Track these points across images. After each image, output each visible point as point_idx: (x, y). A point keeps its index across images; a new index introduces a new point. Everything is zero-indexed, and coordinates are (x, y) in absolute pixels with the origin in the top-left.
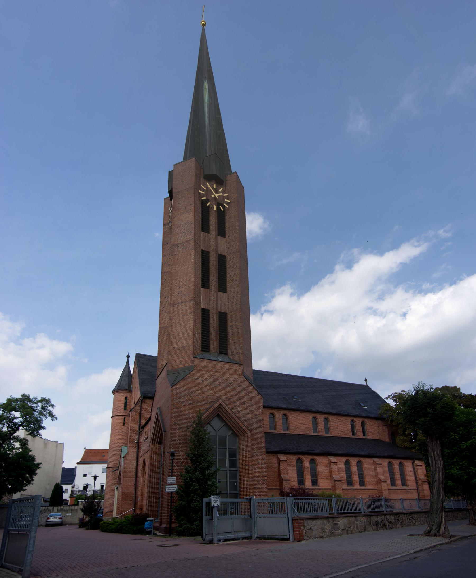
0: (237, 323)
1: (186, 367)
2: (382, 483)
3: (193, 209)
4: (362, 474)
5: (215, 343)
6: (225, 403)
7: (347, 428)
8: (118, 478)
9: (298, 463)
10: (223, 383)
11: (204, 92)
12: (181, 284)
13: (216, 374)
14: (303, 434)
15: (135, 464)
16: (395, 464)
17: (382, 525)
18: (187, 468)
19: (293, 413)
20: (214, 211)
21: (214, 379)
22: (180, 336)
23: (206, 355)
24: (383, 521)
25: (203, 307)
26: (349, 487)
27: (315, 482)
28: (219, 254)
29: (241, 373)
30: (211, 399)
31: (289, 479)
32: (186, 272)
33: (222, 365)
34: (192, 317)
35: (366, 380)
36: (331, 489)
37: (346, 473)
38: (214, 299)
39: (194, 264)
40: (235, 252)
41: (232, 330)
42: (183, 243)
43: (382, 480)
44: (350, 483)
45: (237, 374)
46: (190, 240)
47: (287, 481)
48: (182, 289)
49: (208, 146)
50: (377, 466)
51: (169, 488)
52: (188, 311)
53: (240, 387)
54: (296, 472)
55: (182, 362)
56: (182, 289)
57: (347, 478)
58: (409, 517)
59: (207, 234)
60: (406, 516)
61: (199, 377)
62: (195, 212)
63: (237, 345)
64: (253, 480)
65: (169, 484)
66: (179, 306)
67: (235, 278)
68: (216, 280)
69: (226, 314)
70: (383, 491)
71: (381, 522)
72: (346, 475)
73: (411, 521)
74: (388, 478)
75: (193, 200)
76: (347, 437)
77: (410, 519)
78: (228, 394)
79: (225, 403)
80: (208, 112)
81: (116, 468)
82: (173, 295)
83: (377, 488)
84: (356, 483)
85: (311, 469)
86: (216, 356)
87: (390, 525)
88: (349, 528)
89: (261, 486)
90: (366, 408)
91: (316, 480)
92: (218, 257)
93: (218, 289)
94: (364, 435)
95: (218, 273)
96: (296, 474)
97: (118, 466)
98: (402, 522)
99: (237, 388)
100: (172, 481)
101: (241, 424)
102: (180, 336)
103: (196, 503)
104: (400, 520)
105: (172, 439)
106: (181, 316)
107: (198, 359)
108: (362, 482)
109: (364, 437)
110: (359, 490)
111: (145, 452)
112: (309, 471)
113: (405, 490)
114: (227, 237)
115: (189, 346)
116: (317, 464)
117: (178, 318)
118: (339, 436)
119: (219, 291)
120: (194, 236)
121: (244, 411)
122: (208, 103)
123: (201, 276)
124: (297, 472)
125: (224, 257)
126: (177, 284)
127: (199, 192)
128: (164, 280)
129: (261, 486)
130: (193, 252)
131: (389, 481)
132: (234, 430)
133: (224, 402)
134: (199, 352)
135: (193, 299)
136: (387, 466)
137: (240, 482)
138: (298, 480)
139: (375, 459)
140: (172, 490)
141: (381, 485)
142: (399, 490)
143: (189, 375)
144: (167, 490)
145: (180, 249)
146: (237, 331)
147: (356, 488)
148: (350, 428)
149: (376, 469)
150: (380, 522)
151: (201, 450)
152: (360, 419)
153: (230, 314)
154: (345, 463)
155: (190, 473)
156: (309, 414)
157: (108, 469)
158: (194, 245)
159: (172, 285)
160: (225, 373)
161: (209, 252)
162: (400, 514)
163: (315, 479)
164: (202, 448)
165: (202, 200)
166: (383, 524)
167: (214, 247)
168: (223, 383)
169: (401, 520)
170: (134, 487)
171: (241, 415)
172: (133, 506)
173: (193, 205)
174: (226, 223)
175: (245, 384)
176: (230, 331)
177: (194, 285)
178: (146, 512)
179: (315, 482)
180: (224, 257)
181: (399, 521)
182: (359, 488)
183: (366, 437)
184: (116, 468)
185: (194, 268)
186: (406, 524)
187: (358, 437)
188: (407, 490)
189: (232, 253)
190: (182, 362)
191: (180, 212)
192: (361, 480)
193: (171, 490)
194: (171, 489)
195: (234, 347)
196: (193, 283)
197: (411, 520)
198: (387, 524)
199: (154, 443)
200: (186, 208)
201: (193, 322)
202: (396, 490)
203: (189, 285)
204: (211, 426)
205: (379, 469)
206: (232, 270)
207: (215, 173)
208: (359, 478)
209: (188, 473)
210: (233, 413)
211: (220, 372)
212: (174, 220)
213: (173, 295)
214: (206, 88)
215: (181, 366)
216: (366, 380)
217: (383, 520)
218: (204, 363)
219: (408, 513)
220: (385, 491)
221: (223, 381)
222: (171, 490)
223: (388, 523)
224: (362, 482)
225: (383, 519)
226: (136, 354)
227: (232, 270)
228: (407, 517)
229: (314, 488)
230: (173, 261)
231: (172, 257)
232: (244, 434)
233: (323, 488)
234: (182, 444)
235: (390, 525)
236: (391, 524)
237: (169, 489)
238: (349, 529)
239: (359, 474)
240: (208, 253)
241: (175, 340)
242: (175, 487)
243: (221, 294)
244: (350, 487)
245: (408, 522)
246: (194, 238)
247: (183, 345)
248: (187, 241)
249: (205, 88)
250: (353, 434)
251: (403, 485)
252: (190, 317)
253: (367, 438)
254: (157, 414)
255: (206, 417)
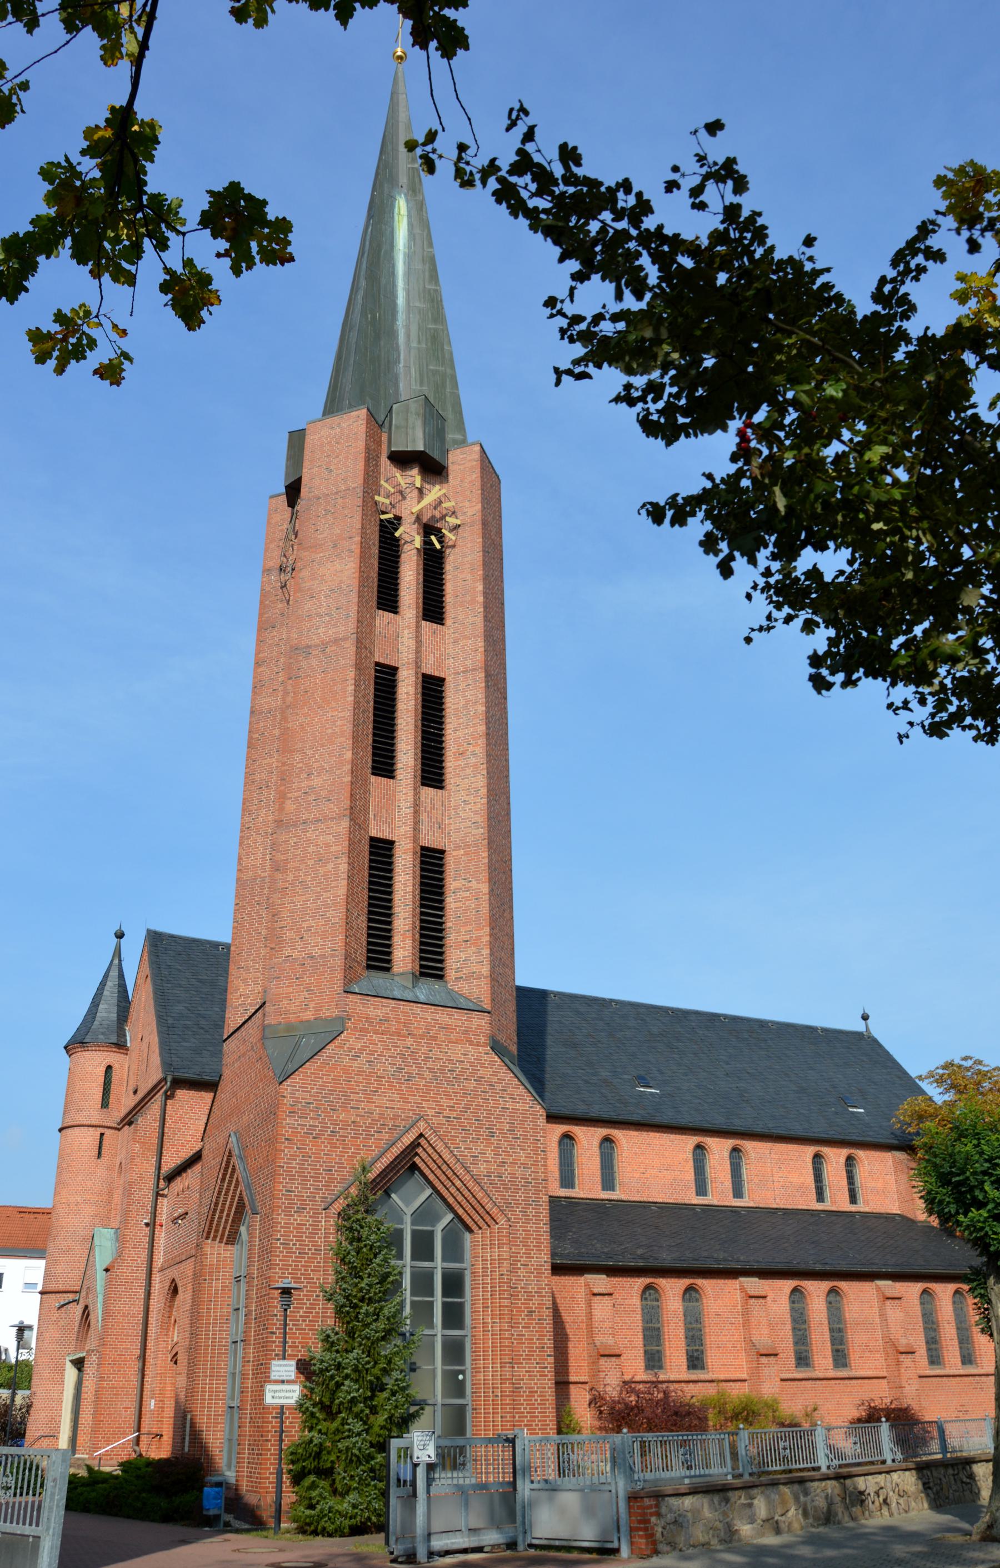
0: (474, 884)
1: (320, 1018)
2: (902, 1358)
3: (358, 551)
4: (840, 1330)
5: (409, 942)
6: (435, 1132)
7: (802, 1180)
8: (76, 1329)
9: (646, 1299)
10: (431, 1070)
11: (396, 223)
12: (314, 765)
13: (410, 1041)
14: (666, 1201)
15: (141, 1293)
16: (941, 1295)
17: (877, 1504)
18: (328, 1336)
19: (636, 1133)
20: (415, 551)
21: (402, 1055)
22: (305, 925)
23: (378, 979)
24: (881, 1491)
25: (374, 833)
26: (801, 1372)
27: (695, 1361)
28: (424, 676)
29: (483, 1040)
30: (395, 1118)
31: (617, 1352)
32: (330, 731)
33: (429, 1014)
34: (344, 867)
35: (865, 1018)
36: (745, 1380)
37: (794, 1329)
38: (408, 811)
39: (355, 709)
40: (472, 670)
41: (460, 904)
42: (325, 645)
43: (902, 1349)
44: (803, 1360)
45: (471, 1043)
46: (345, 639)
47: (614, 1359)
48: (317, 782)
49: (401, 365)
50: (888, 1302)
51: (275, 1391)
52: (333, 849)
53: (479, 1080)
54: (640, 1329)
55: (312, 1005)
56: (317, 782)
57: (796, 1343)
58: (961, 1475)
59: (391, 615)
60: (950, 1471)
61: (361, 1051)
62: (363, 557)
63: (473, 949)
64: (513, 1367)
65: (276, 1382)
66: (304, 831)
67: (471, 748)
68: (416, 754)
69: (443, 852)
70: (904, 1384)
71: (877, 1493)
72: (794, 1335)
73: (966, 1488)
74: (918, 1341)
75: (359, 526)
76: (800, 1207)
77: (962, 1482)
78: (444, 1102)
79: (435, 1132)
80: (404, 274)
81: (71, 1297)
82: (289, 795)
83: (885, 1374)
84: (823, 1361)
85: (685, 1319)
86: (410, 986)
87: (901, 1501)
88: (782, 1515)
89: (536, 1384)
90: (862, 1111)
91: (702, 1352)
92: (423, 681)
93: (419, 778)
94: (853, 1199)
95: (420, 732)
96: (640, 1336)
97: (77, 1288)
98: (938, 1492)
99: (472, 1085)
100: (284, 1374)
101: (480, 1195)
102: (305, 925)
103: (354, 1440)
104: (931, 1484)
105: (279, 1239)
106: (311, 863)
107: (359, 996)
108: (840, 1357)
109: (853, 1208)
110: (833, 1382)
111: (178, 1260)
112: (681, 1324)
113: (971, 1378)
114: (449, 621)
115: (332, 956)
116: (705, 1301)
117: (303, 867)
118: (775, 1206)
119: (423, 784)
120: (358, 627)
121: (490, 1154)
122: (405, 253)
123: (371, 741)
124: (645, 1330)
125: (441, 681)
126: (301, 765)
127: (373, 498)
128: (257, 736)
129: (536, 1384)
130: (351, 674)
131: (922, 1352)
132: (460, 1211)
133: (432, 1128)
134: (360, 969)
135: (347, 812)
136: (917, 1302)
137: (476, 1370)
138: (645, 1352)
139: (881, 1283)
140: (284, 1398)
141: (898, 1363)
142: (951, 1379)
143: (331, 1047)
144: (269, 1400)
145: (314, 663)
146: (473, 906)
147: (820, 1375)
148: (810, 1180)
149: (883, 1315)
150: (872, 1494)
151: (366, 1281)
152: (841, 1150)
153: (454, 853)
154: (790, 1297)
155: (337, 1351)
156: (684, 1137)
157: (45, 1296)
158: (357, 654)
159: (287, 768)
160: (434, 1038)
161: (396, 669)
162: (933, 1469)
163: (697, 1350)
164: (369, 1275)
165: (381, 520)
166: (881, 1499)
167: (410, 656)
168: (431, 1070)
169: (935, 1485)
170: (137, 1365)
171: (481, 1169)
172: (134, 1425)
173: (358, 539)
174: (448, 584)
175: (495, 1074)
176: (453, 905)
177: (352, 772)
178: (183, 1449)
179: (695, 1361)
180: (441, 681)
181: (930, 1488)
182: (831, 1374)
183: (861, 1207)
184: (71, 1297)
185: (354, 720)
186: (951, 1496)
187: (834, 1208)
188: (977, 1378)
189: (463, 672)
190: (312, 1005)
191: (318, 556)
192: (837, 1351)
193: (280, 1398)
194: (281, 1394)
195: (463, 956)
196: (349, 767)
197: (967, 1484)
198: (893, 1498)
199: (214, 1239)
200: (335, 547)
201: (345, 882)
202: (945, 1379)
203: (338, 772)
204: (53, 12)
205: (894, 1312)
206: (462, 721)
207: (422, 449)
208: (833, 1345)
209: (329, 1350)
210: (458, 1160)
211: (422, 1037)
212: (301, 575)
213: (289, 795)
214: (402, 212)
215: (309, 1015)
216: (865, 1018)
217: (882, 1488)
218: (378, 1009)
219: (956, 1464)
220: (911, 1382)
221: (430, 1064)
222: (280, 1398)
223: (897, 1497)
224: (840, 1357)
225: (883, 1485)
226: (149, 931)
227: (462, 721)
228: (954, 1475)
229: (693, 1377)
230: (292, 694)
231: (290, 681)
232: (489, 1226)
233: (722, 1377)
234: (307, 1254)
235: (901, 1501)
236: (905, 1498)
237: (277, 1394)
238: (783, 1518)
239: (831, 1330)
240: (393, 670)
241: (289, 935)
242: (294, 1391)
243: (428, 792)
244: (805, 1372)
245: (955, 1491)
246: (358, 633)
247: (316, 951)
248: (336, 641)
249: (399, 214)
250: (820, 1197)
251: (963, 1363)
252: (336, 868)
253: (862, 1210)
254: (227, 1153)
255: (379, 1175)
